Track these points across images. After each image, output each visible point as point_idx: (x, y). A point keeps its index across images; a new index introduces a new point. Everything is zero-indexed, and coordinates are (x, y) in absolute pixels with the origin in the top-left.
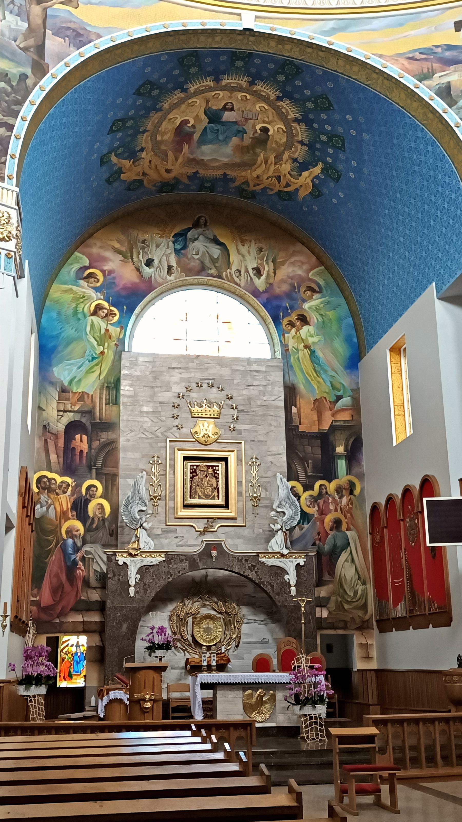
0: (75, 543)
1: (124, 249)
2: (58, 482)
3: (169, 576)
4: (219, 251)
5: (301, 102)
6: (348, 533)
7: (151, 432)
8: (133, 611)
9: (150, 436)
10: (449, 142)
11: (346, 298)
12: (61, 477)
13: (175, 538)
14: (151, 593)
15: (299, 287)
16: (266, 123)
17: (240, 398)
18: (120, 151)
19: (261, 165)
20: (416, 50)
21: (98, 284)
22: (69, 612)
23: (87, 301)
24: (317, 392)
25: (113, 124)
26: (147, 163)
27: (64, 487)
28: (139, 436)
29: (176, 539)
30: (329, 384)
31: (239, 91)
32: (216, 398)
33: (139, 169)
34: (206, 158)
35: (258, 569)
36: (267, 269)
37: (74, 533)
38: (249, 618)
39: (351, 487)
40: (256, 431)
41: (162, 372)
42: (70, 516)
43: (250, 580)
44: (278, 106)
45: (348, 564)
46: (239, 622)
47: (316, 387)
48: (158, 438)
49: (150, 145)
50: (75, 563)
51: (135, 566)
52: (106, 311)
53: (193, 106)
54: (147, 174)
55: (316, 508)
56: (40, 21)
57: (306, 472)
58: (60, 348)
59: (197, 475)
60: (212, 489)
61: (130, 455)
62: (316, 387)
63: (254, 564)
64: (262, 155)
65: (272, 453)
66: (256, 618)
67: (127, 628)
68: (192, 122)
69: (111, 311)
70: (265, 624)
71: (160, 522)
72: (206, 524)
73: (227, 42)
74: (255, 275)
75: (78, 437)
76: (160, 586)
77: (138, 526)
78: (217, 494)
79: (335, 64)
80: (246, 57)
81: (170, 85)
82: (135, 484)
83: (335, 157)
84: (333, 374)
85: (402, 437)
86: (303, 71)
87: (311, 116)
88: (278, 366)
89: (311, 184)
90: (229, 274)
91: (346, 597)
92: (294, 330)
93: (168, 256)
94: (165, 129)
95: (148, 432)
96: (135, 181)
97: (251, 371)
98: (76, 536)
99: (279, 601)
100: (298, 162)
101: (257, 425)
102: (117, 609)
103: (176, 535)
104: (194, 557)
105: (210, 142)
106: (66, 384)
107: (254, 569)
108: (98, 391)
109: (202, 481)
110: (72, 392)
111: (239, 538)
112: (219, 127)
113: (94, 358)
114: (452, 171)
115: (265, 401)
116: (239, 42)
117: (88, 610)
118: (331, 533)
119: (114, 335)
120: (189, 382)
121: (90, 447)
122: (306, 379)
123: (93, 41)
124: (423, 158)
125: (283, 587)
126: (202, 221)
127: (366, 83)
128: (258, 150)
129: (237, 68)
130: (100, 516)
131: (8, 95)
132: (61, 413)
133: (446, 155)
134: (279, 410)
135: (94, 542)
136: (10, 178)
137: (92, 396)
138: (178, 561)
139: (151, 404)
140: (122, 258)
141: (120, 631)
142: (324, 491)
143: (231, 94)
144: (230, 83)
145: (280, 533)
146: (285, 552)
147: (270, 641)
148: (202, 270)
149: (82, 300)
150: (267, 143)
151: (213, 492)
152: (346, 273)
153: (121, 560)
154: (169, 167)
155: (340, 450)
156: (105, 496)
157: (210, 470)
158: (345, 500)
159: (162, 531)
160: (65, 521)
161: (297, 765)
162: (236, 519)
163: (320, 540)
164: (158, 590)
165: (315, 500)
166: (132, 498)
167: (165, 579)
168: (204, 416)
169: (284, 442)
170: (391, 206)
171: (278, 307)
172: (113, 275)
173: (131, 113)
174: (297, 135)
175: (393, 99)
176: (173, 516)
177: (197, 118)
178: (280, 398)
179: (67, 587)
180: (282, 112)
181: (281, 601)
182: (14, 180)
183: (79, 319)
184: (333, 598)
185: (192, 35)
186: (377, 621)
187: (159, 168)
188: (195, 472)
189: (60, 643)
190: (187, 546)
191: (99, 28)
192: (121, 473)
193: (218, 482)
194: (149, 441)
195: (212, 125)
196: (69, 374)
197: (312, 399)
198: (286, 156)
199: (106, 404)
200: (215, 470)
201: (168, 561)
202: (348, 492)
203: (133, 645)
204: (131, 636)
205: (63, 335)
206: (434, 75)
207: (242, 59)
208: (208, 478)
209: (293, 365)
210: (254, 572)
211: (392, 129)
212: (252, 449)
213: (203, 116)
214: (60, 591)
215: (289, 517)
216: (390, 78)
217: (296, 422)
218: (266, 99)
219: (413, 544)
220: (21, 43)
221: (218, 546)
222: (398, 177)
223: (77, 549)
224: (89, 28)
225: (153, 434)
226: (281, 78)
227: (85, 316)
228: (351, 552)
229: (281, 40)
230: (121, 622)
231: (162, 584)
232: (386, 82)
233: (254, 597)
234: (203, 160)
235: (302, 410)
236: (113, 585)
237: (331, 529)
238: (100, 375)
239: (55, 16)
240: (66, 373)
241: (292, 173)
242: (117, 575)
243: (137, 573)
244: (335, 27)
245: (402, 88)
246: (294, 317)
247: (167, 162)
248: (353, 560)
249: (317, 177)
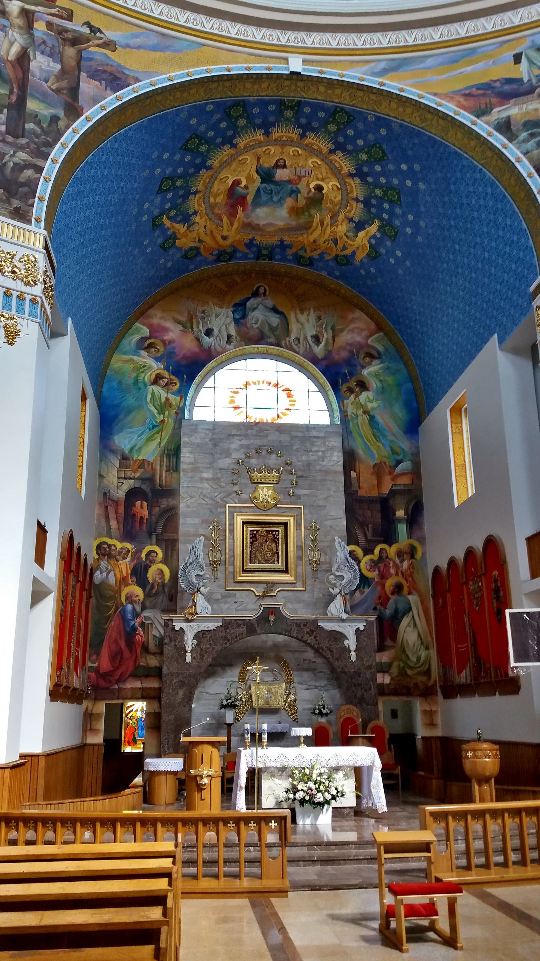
0: (134, 609)
1: (183, 319)
2: (118, 548)
4: (278, 320)
5: (354, 154)
6: (410, 597)
7: (211, 498)
9: (210, 502)
10: (510, 179)
11: (405, 364)
12: (121, 543)
13: (235, 602)
15: (358, 353)
16: (320, 180)
17: (300, 463)
18: (172, 213)
19: (317, 227)
20: (472, 87)
21: (159, 354)
22: (127, 678)
23: (147, 371)
25: (162, 182)
26: (202, 230)
27: (124, 554)
28: (198, 502)
30: (389, 449)
31: (291, 145)
32: (275, 464)
33: (194, 235)
34: (262, 223)
36: (326, 336)
37: (134, 598)
39: (412, 552)
41: (221, 439)
42: (130, 582)
43: (309, 645)
44: (331, 160)
45: (410, 629)
47: (375, 452)
49: (203, 207)
51: (192, 632)
52: (166, 380)
53: (243, 164)
54: (202, 241)
55: (377, 572)
56: (73, 63)
57: (366, 536)
58: (121, 417)
59: (257, 540)
61: (190, 521)
62: (375, 452)
63: (312, 629)
64: (317, 217)
65: (330, 517)
68: (244, 183)
69: (171, 380)
71: (219, 586)
74: (313, 342)
75: (138, 503)
77: (195, 590)
78: (276, 559)
80: (295, 105)
81: (219, 140)
82: (193, 549)
83: (391, 213)
84: (393, 438)
85: (464, 498)
86: (354, 118)
87: (365, 169)
88: (336, 432)
89: (368, 245)
90: (288, 343)
91: (409, 662)
92: (352, 397)
93: (227, 326)
94: (218, 190)
96: (191, 249)
97: (310, 437)
98: (135, 602)
99: (339, 667)
100: (353, 221)
103: (235, 600)
104: (252, 622)
105: (265, 204)
106: (127, 452)
108: (159, 459)
109: (262, 544)
110: (133, 459)
112: (272, 187)
113: (154, 427)
114: (514, 212)
116: (287, 88)
117: (147, 676)
118: (393, 599)
119: (174, 403)
120: (249, 448)
121: (150, 514)
122: (366, 444)
123: (132, 85)
124: (482, 202)
126: (261, 290)
127: (421, 126)
128: (313, 212)
129: (287, 119)
130: (159, 581)
131: (37, 136)
132: (122, 481)
133: (507, 194)
135: (154, 607)
136: (38, 220)
137: (152, 463)
138: (235, 625)
139: (211, 471)
140: (182, 328)
142: (385, 555)
143: (282, 149)
144: (280, 137)
145: (339, 597)
146: (345, 616)
148: (260, 339)
149: (142, 370)
150: (321, 203)
151: (272, 556)
152: (405, 338)
153: (178, 626)
154: (225, 233)
155: (400, 513)
156: (165, 561)
157: (270, 535)
158: (406, 564)
160: (125, 587)
161: (345, 860)
162: (295, 583)
163: (381, 604)
165: (374, 564)
166: (190, 563)
168: (263, 481)
170: (449, 259)
171: (337, 374)
172: (173, 345)
173: (180, 170)
174: (352, 191)
175: (450, 140)
176: (232, 581)
177: (249, 178)
179: (126, 653)
180: (336, 167)
182: (43, 223)
183: (140, 389)
184: (395, 664)
186: (441, 687)
187: (215, 234)
189: (125, 708)
190: (247, 610)
191: (138, 72)
192: (181, 538)
193: (277, 546)
195: (265, 185)
196: (129, 442)
197: (372, 464)
198: (341, 216)
199: (166, 471)
202: (410, 555)
205: (123, 404)
206: (492, 110)
207: (292, 108)
210: (312, 637)
211: (449, 175)
212: (312, 514)
213: (255, 175)
214: (119, 657)
216: (445, 117)
217: (355, 487)
218: (318, 153)
219: (477, 608)
220: (53, 84)
221: (275, 611)
222: (455, 227)
223: (136, 615)
224: (127, 72)
226: (332, 128)
227: (145, 385)
228: (413, 617)
229: (331, 83)
232: (441, 122)
233: (315, 662)
234: (258, 225)
235: (361, 475)
237: (393, 593)
238: (160, 442)
239: (91, 59)
240: (127, 441)
241: (348, 234)
243: (193, 639)
244: (387, 67)
245: (459, 127)
246: (353, 383)
247: (222, 227)
248: (415, 625)
249: (374, 237)
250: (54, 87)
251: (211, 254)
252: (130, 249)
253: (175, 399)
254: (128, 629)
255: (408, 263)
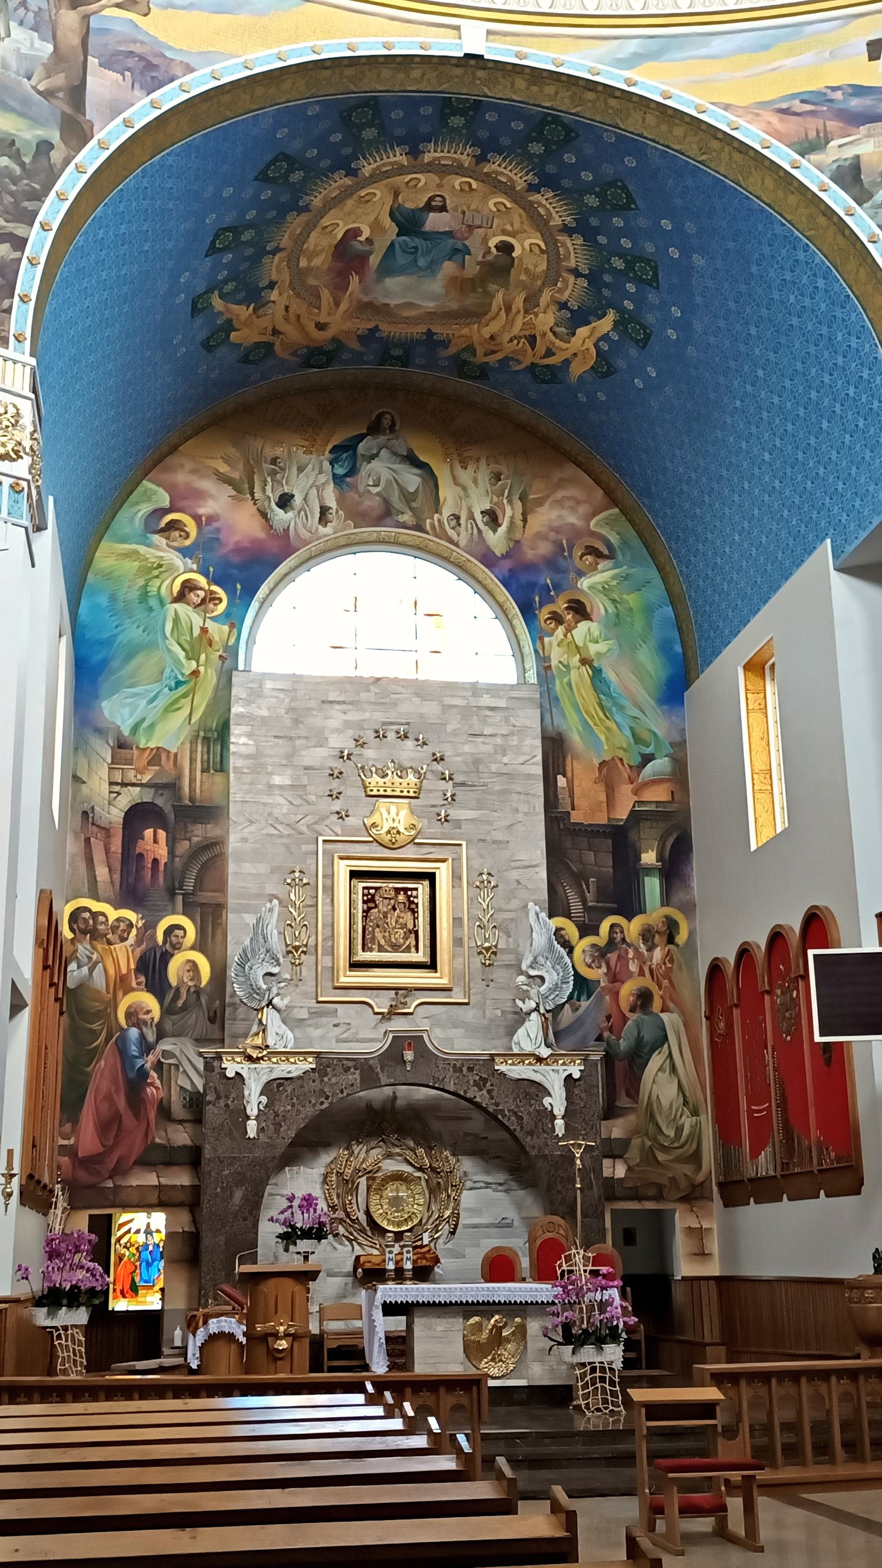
0: (142, 1036)
1: (236, 475)
2: (111, 919)
3: (322, 1099)
5: (575, 195)
6: (665, 1016)
7: (288, 825)
8: (255, 1166)
9: (286, 831)
10: (858, 270)
11: (660, 569)
12: (116, 909)
13: (335, 1026)
14: (289, 1132)
15: (571, 548)
16: (509, 234)
17: (459, 759)
18: (229, 287)
19: (498, 314)
20: (793, 96)
21: (188, 542)
22: (131, 1168)
23: (166, 574)
24: (606, 748)
25: (216, 236)
26: (280, 312)
27: (122, 929)
28: (265, 832)
29: (335, 1028)
30: (628, 733)
31: (457, 174)
32: (412, 759)
33: (265, 323)
34: (393, 302)
35: (492, 1085)
36: (510, 512)
37: (142, 1016)
38: (474, 1180)
39: (671, 930)
40: (489, 822)
41: (309, 709)
42: (134, 984)
43: (478, 1106)
44: (531, 203)
45: (664, 1077)
46: (455, 1186)
47: (603, 738)
48: (301, 836)
49: (286, 276)
50: (143, 1074)
51: (257, 1080)
52: (202, 594)
53: (368, 201)
54: (280, 333)
55: (604, 969)
56: (76, 41)
57: (584, 901)
58: (115, 664)
59: (376, 906)
60: (405, 933)
61: (248, 868)
62: (603, 738)
63: (484, 1076)
64: (500, 296)
65: (519, 864)
66: (489, 1179)
67: (242, 1198)
68: (366, 233)
69: (212, 592)
70: (506, 1191)
71: (305, 995)
72: (393, 1000)
73: (434, 81)
74: (486, 524)
75: (149, 833)
76: (306, 1117)
77: (264, 1003)
78: (413, 943)
79: (640, 122)
80: (470, 109)
81: (325, 163)
82: (258, 923)
84: (636, 713)
85: (767, 834)
86: (578, 136)
87: (594, 222)
88: (530, 699)
89: (593, 351)
90: (436, 523)
91: (661, 1138)
92: (561, 630)
93: (320, 489)
94: (316, 246)
95: (282, 823)
96: (258, 344)
97: (479, 708)
98: (145, 1023)
99: (533, 1147)
100: (568, 309)
101: (491, 811)
102: (223, 1161)
103: (336, 1021)
104: (371, 1062)
105: (401, 271)
106: (126, 732)
107: (485, 1086)
108: (188, 746)
110: (138, 748)
111: (456, 1026)
112: (417, 242)
113: (179, 684)
114: (863, 327)
115: (505, 764)
116: (457, 80)
117: (169, 1164)
118: (633, 1017)
119: (217, 638)
120: (362, 729)
121: (171, 853)
122: (585, 723)
123: (178, 77)
124: (807, 302)
125: (540, 1120)
126: (386, 422)
127: (700, 159)
128: (492, 287)
129: (453, 130)
130: (190, 983)
131: (15, 181)
132: (117, 788)
133: (852, 296)
134: (533, 782)
135: (179, 1034)
136: (19, 339)
137: (176, 755)
138: (339, 1070)
139: (289, 771)
140: (234, 493)
141: (229, 1203)
142: (619, 937)
143: (442, 179)
144: (438, 159)
145: (534, 1016)
146: (545, 1052)
147: (516, 1224)
148: (385, 515)
149: (156, 572)
150: (509, 272)
151: (406, 938)
152: (660, 522)
153: (231, 1068)
154: (323, 319)
155: (649, 858)
156: (200, 946)
157: (401, 897)
158: (658, 954)
159: (309, 1013)
160: (125, 994)
162: (450, 990)
163: (611, 1030)
164: (302, 1126)
165: (600, 953)
166: (253, 950)
167: (315, 1105)
168: (389, 793)
169: (543, 844)
170: (746, 392)
171: (531, 586)
172: (216, 525)
173: (251, 215)
174: (567, 258)
175: (751, 189)
176: (330, 984)
177: (376, 225)
178: (535, 760)
179: (128, 1119)
180: (539, 214)
181: (537, 1146)
182: (28, 343)
183: (151, 609)
184: (636, 1142)
185: (367, 67)
186: (720, 1185)
187: (303, 320)
188: (372, 900)
189: (115, 1227)
190: (358, 1041)
191: (189, 53)
192: (231, 901)
193: (415, 918)
194: (284, 841)
195: (405, 238)
196: (131, 714)
197: (596, 762)
198: (545, 298)
199: (202, 771)
200: (411, 896)
201: (321, 1070)
202: (665, 938)
203: (255, 1230)
204: (250, 1212)
205: (120, 639)
206: (828, 143)
207: (462, 113)
208: (398, 911)
209: (559, 696)
210: (484, 1092)
211: (748, 247)
212: (482, 857)
213: (387, 222)
214: (115, 1128)
215: (551, 986)
216: (744, 148)
217: (565, 804)
218: (508, 190)
219: (789, 1038)
220: (39, 82)
221: (416, 1041)
222: (759, 338)
223: (146, 1048)
224: (169, 54)
225: (293, 829)
226: (537, 148)
227: (162, 604)
228: (670, 1054)
229: (537, 75)
230: (231, 1187)
231: (309, 1113)
232: (737, 156)
233: (485, 1138)
234: (387, 305)
235: (576, 783)
236: (216, 1115)
237: (632, 1010)
238: (190, 714)
239: (105, 31)
240: (126, 711)
241: (558, 330)
242: (223, 1096)
243: (261, 1094)
244: (640, 51)
245: (768, 168)
246: (561, 605)
247: (319, 308)
248: (673, 1069)
249: (605, 337)
250: (41, 87)
251: (294, 354)
252: (147, 355)
253: (220, 632)
254: (132, 1075)
255: (668, 390)
